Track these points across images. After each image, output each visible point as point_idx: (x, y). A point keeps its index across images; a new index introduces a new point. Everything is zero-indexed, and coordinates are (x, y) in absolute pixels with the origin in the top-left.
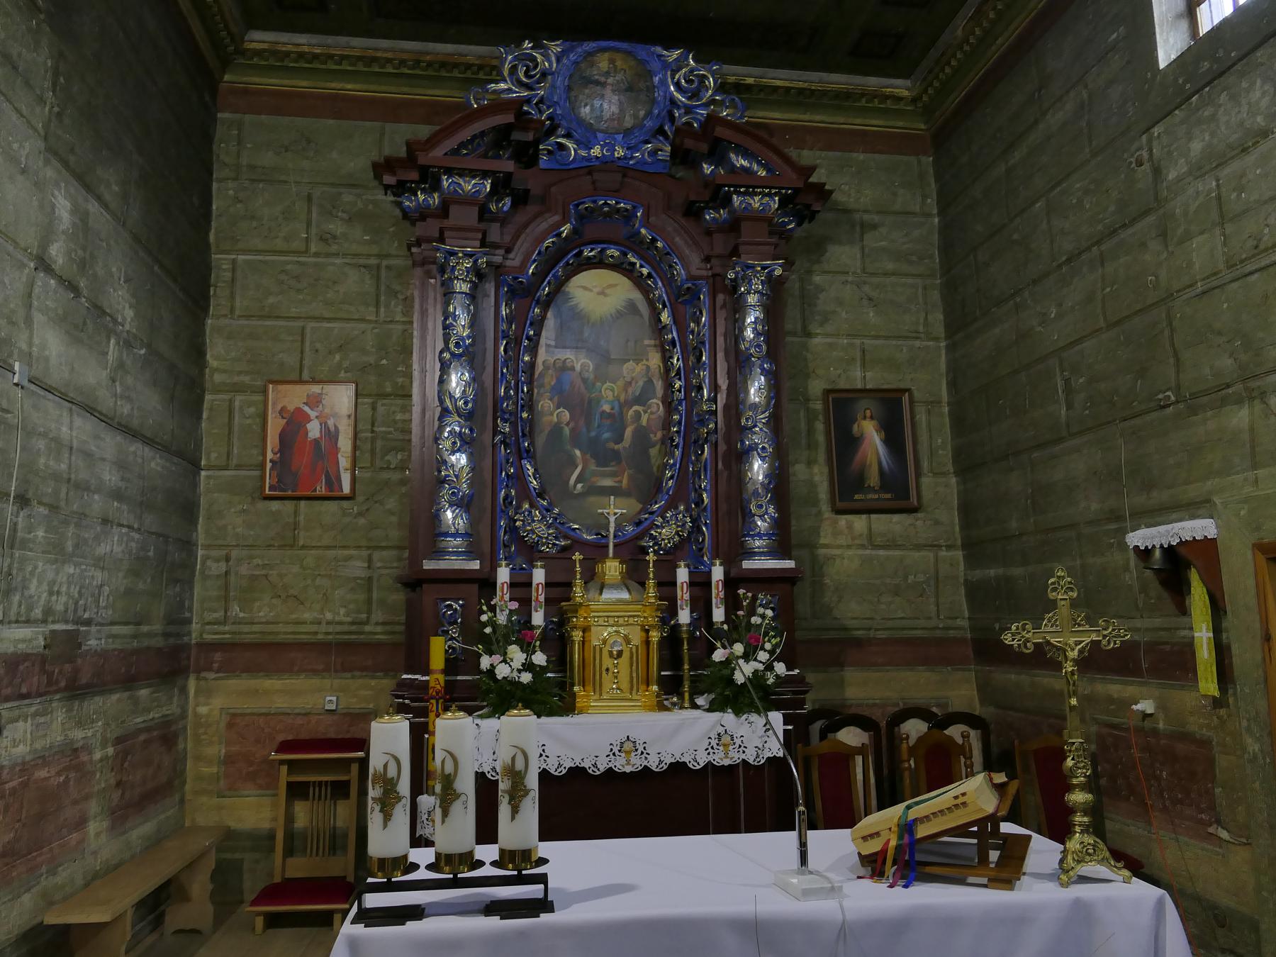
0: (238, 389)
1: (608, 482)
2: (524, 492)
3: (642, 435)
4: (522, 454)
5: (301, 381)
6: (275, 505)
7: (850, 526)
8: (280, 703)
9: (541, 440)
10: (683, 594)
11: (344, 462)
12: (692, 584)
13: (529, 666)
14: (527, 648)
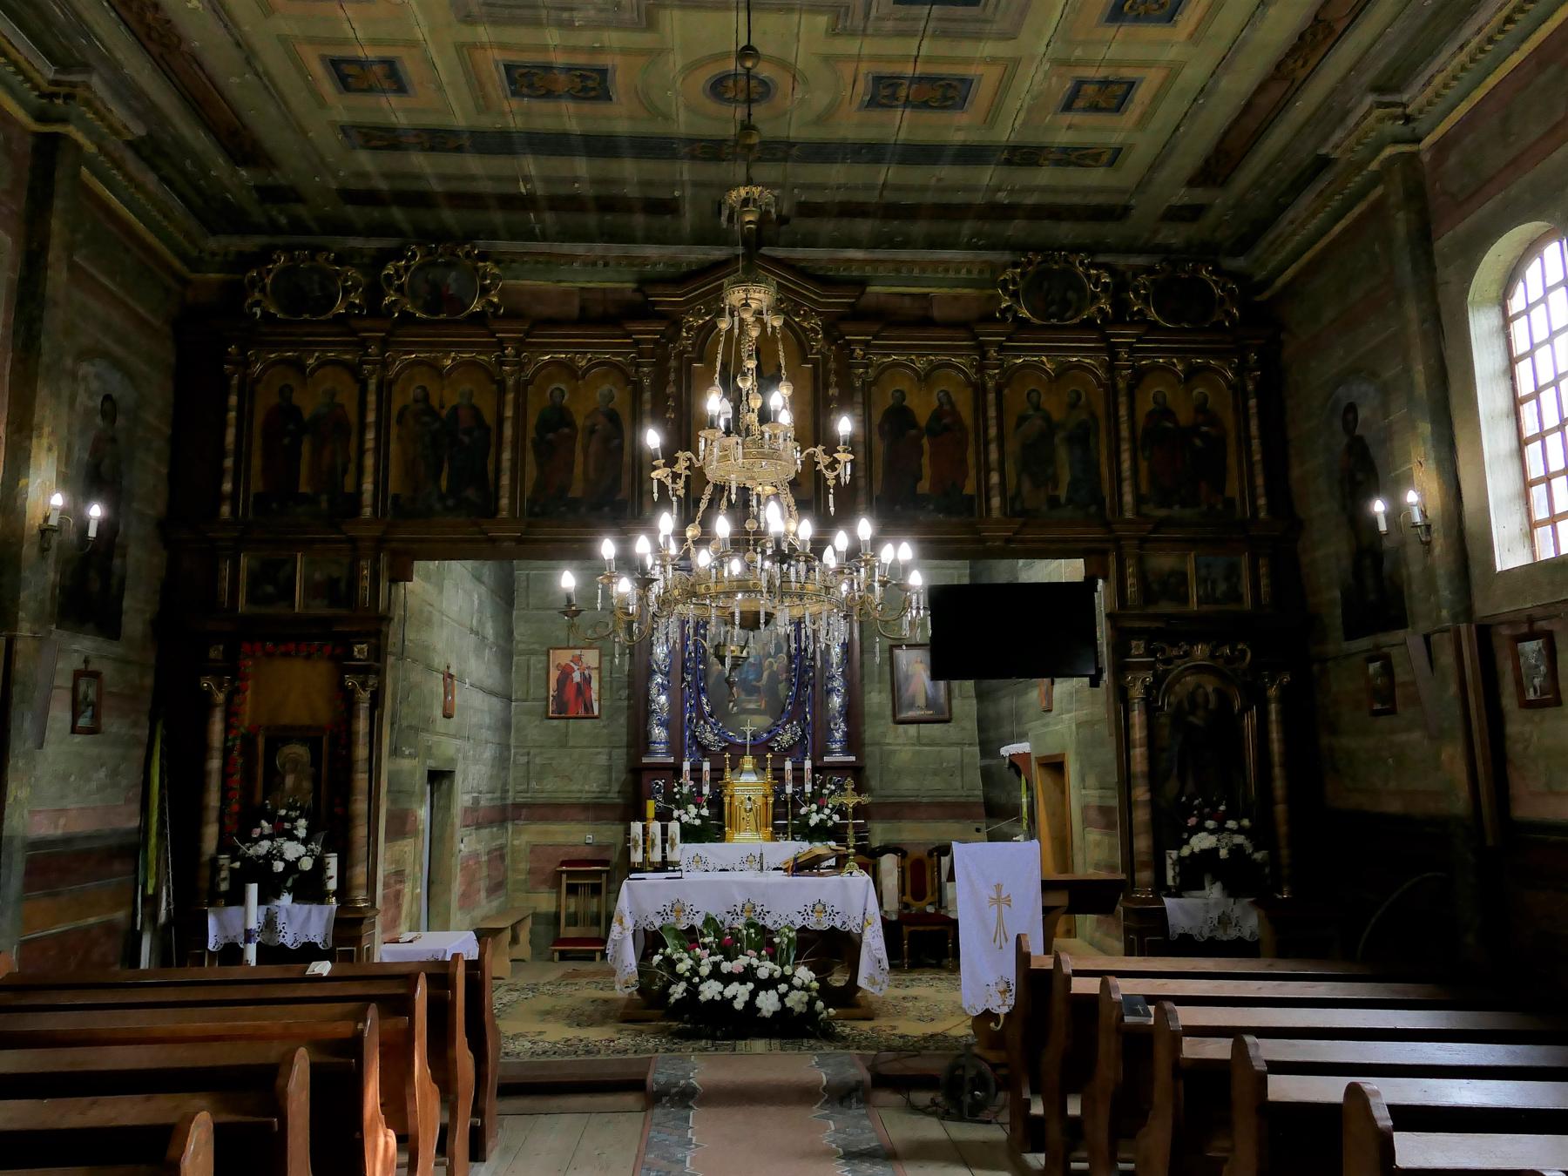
0: (533, 653)
1: (752, 706)
2: (701, 715)
3: (773, 677)
4: (701, 691)
5: (568, 648)
6: (555, 722)
7: (906, 732)
8: (560, 839)
9: (711, 681)
10: (789, 776)
11: (594, 696)
12: (794, 769)
13: (699, 816)
14: (699, 806)
